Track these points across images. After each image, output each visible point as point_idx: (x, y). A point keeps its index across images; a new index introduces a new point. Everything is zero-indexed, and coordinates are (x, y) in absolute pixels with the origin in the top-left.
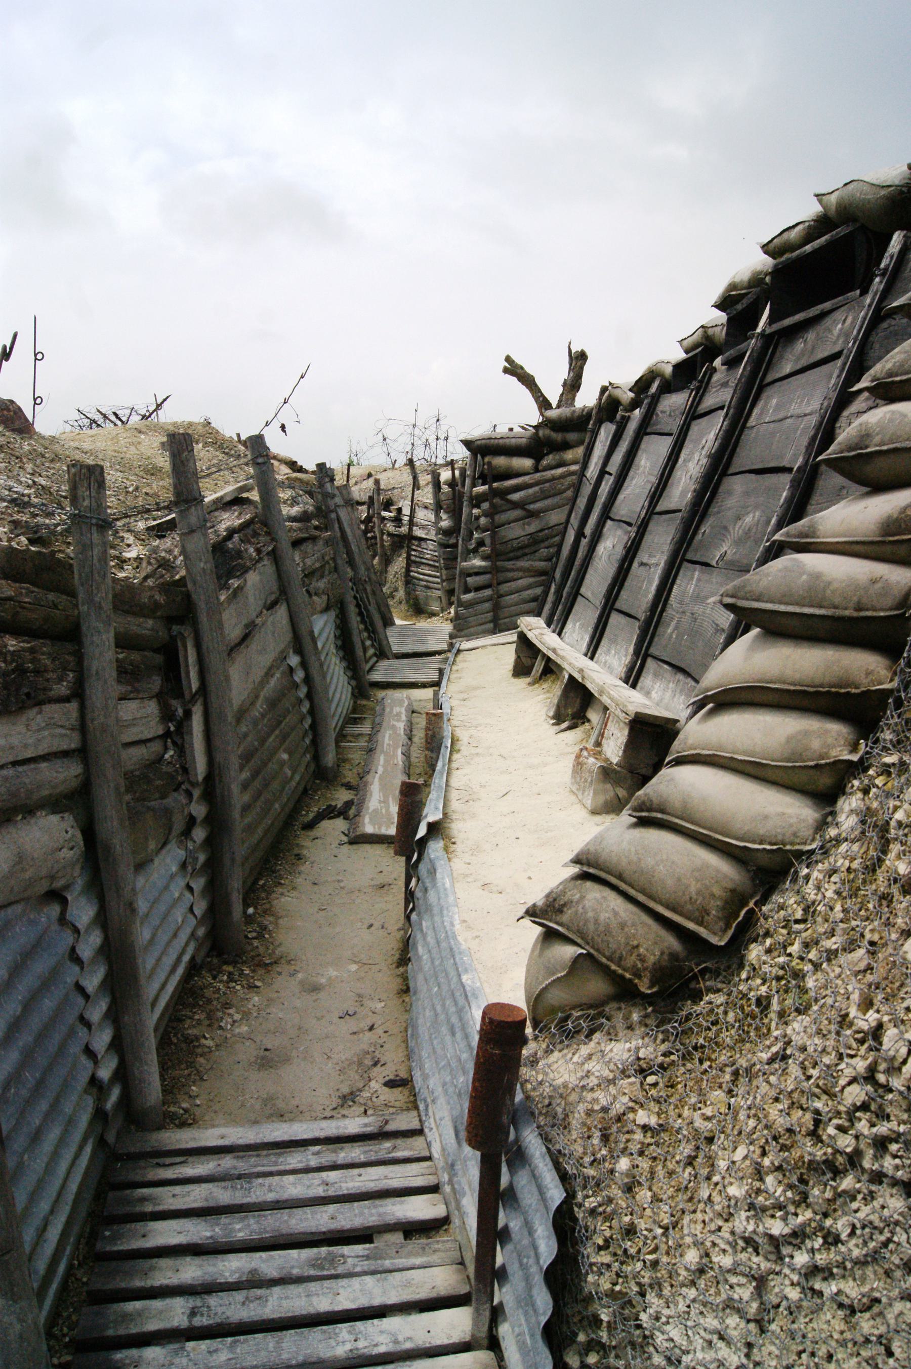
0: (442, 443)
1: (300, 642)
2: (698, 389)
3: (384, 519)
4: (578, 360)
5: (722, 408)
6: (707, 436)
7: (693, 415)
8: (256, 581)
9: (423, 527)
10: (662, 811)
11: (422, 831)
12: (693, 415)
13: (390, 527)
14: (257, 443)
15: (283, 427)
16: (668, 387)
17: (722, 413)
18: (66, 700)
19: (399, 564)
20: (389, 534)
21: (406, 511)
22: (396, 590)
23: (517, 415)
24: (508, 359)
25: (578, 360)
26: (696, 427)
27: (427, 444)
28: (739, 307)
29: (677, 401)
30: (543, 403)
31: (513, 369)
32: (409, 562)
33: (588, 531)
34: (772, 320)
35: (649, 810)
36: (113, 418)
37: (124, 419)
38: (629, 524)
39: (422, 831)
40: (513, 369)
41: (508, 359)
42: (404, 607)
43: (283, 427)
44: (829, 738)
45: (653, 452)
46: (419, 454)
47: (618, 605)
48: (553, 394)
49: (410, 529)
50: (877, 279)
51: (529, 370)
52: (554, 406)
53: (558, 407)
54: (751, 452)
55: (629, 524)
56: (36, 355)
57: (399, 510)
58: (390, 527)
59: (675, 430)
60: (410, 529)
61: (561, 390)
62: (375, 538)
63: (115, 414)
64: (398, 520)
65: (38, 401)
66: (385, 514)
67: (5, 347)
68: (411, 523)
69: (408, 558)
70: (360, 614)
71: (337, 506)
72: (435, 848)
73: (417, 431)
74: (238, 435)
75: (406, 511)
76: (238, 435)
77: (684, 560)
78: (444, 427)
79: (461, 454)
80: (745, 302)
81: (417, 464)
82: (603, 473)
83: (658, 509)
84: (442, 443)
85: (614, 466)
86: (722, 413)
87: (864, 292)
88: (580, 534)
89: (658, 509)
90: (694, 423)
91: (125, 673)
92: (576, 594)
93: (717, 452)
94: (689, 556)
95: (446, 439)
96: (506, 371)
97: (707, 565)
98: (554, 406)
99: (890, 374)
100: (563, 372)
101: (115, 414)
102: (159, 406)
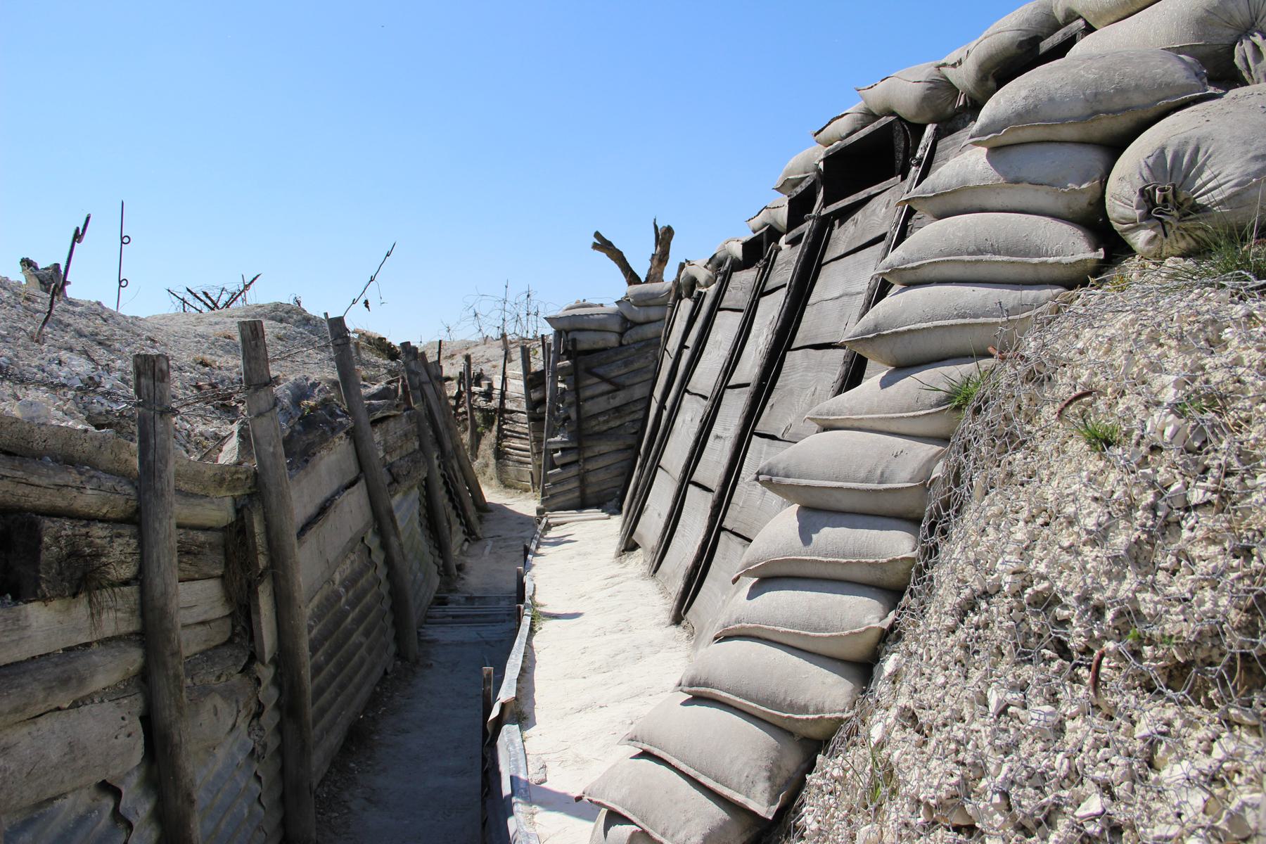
0: (532, 318)
1: (381, 520)
2: (765, 267)
3: (475, 394)
4: (664, 238)
5: (784, 286)
6: (771, 309)
7: (761, 292)
8: (335, 458)
9: (514, 400)
10: (706, 685)
11: (495, 712)
12: (761, 292)
13: (481, 402)
14: (337, 324)
15: (366, 303)
16: (738, 266)
17: (784, 290)
18: (126, 583)
19: (490, 438)
20: (481, 409)
21: (497, 385)
22: (487, 465)
23: (606, 291)
24: (597, 235)
25: (664, 238)
26: (765, 302)
27: (518, 319)
28: (799, 190)
29: (747, 277)
30: (633, 278)
31: (603, 245)
32: (501, 436)
33: (668, 403)
34: (827, 202)
35: (699, 685)
36: (203, 297)
37: (214, 299)
38: (705, 398)
39: (495, 712)
40: (603, 245)
41: (597, 235)
42: (495, 482)
43: (366, 303)
44: (861, 613)
45: (726, 327)
46: (509, 329)
47: (695, 478)
48: (642, 271)
49: (502, 403)
50: (914, 168)
51: (618, 245)
52: (643, 280)
53: (647, 281)
54: (812, 325)
55: (705, 398)
56: (122, 239)
57: (491, 386)
58: (481, 402)
59: (745, 306)
60: (502, 403)
61: (649, 264)
62: (465, 413)
63: (205, 294)
64: (488, 395)
65: (124, 283)
66: (474, 389)
67: (78, 229)
68: (503, 395)
69: (500, 430)
70: (448, 491)
71: (421, 383)
72: (509, 732)
73: (508, 307)
74: (326, 314)
75: (497, 385)
76: (326, 314)
77: (753, 433)
78: (534, 304)
79: (549, 331)
80: (804, 185)
81: (509, 338)
82: (682, 346)
83: (731, 383)
84: (532, 318)
85: (690, 342)
86: (784, 290)
87: (904, 178)
88: (662, 407)
89: (731, 383)
90: (762, 299)
91: (185, 551)
92: (656, 466)
93: (781, 327)
94: (759, 428)
95: (536, 314)
96: (595, 246)
97: (773, 438)
98: (643, 280)
99: (905, 261)
100: (650, 248)
101: (205, 294)
102: (247, 287)
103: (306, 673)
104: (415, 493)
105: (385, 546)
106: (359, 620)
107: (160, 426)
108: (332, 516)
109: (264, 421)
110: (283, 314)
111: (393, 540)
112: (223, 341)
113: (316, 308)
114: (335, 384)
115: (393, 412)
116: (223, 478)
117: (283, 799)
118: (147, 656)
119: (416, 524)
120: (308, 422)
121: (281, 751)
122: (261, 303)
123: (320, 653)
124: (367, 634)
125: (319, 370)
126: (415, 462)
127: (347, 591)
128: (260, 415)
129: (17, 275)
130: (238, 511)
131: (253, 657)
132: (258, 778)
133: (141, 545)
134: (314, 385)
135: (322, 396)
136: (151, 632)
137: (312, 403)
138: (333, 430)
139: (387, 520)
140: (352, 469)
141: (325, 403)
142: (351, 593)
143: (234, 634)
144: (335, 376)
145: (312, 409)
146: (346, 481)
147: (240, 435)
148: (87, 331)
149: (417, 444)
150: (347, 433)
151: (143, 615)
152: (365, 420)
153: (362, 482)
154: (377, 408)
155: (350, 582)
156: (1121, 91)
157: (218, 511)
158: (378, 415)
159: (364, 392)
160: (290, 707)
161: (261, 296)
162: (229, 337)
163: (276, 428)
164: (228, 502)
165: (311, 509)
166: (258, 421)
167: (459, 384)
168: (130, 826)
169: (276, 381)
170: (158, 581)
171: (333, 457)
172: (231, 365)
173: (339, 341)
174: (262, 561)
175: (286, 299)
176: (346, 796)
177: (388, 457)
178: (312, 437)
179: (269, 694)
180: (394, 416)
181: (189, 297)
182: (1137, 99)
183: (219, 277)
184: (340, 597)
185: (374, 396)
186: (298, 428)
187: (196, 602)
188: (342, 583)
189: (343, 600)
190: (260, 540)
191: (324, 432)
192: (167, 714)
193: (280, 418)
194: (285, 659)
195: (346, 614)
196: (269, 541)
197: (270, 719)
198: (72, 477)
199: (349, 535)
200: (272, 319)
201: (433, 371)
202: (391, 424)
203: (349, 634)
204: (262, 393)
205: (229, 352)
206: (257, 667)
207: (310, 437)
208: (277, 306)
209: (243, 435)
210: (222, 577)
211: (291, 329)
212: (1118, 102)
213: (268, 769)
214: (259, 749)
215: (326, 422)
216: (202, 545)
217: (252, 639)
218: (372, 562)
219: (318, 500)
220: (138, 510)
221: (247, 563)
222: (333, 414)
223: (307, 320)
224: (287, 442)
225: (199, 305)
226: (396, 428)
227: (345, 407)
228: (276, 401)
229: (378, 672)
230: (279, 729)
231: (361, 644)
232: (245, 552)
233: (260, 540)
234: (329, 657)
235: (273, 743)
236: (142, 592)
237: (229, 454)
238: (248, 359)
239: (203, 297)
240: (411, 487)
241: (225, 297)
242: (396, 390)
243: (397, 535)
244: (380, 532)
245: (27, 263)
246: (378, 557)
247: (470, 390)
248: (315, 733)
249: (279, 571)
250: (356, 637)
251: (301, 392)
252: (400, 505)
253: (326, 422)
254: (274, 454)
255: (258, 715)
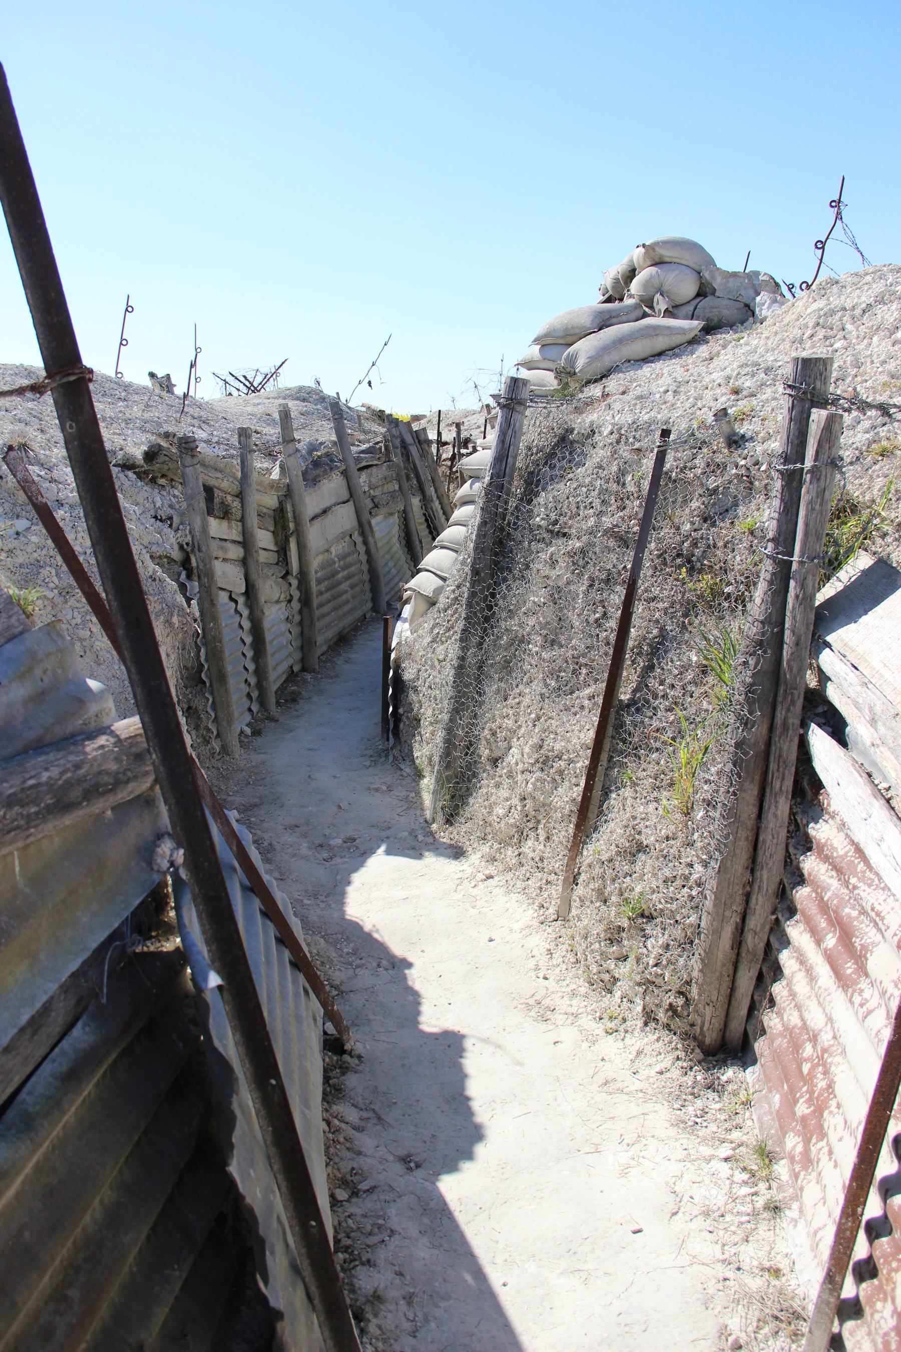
1: (363, 528)
8: (332, 486)
15: (370, 383)
36: (243, 379)
37: (251, 380)
43: (370, 383)
63: (245, 377)
101: (245, 377)
103: (313, 583)
104: (395, 519)
105: (365, 542)
106: (347, 578)
107: (249, 457)
108: (330, 517)
109: (292, 459)
110: (305, 395)
111: (370, 539)
112: (265, 418)
113: (329, 390)
114: (335, 443)
115: (375, 462)
116: (273, 485)
117: (302, 648)
118: (245, 552)
119: (395, 539)
120: (316, 464)
121: (301, 623)
122: (289, 386)
123: (322, 585)
124: (352, 587)
125: (326, 434)
126: (393, 497)
127: (339, 560)
128: (290, 455)
129: (147, 382)
130: (280, 503)
131: (288, 573)
132: (290, 632)
133: (242, 507)
134: (321, 444)
135: (326, 450)
136: (246, 543)
137: (319, 454)
138: (331, 469)
139: (366, 527)
140: (345, 495)
141: (327, 455)
142: (342, 563)
143: (279, 561)
144: (334, 438)
145: (319, 457)
146: (341, 500)
147: (280, 467)
148: (196, 415)
149: (397, 487)
150: (342, 473)
151: (244, 535)
152: (353, 468)
153: (351, 502)
154: (363, 459)
155: (343, 557)
156: (573, 328)
157: (271, 501)
158: (364, 464)
159: (354, 449)
160: (306, 601)
161: (290, 380)
162: (269, 415)
163: (298, 465)
164: (276, 497)
165: (318, 510)
166: (289, 459)
167: (454, 447)
168: (241, 615)
169: (299, 441)
170: (249, 521)
171: (332, 485)
172: (272, 432)
173: (336, 417)
174: (292, 526)
175: (310, 383)
176: (335, 659)
177: (372, 492)
178: (319, 471)
179: (296, 594)
180: (376, 465)
181: (230, 379)
182: (577, 331)
183: (252, 362)
184: (334, 563)
185: (363, 452)
186: (310, 466)
187: (264, 539)
188: (337, 556)
189: (337, 565)
190: (290, 515)
191: (326, 470)
192: (253, 576)
193: (301, 460)
194: (303, 576)
195: (338, 573)
196: (295, 517)
197: (296, 605)
198: (219, 475)
199: (341, 530)
200: (298, 399)
201: (422, 437)
202: (374, 470)
203: (339, 583)
204: (290, 445)
205: (269, 425)
206: (289, 577)
207: (318, 471)
208: (301, 389)
209: (282, 467)
210: (273, 532)
211: (310, 407)
212: (572, 332)
213: (296, 631)
214: (290, 617)
215: (327, 464)
216: (265, 514)
217: (287, 564)
218: (357, 551)
219: (323, 506)
220: (241, 493)
221: (285, 527)
222: (332, 461)
223: (323, 399)
224: (304, 473)
225: (237, 384)
226: (378, 474)
227: (341, 458)
228: (297, 450)
229: (359, 613)
230: (300, 612)
231: (346, 592)
232: (284, 522)
233: (290, 515)
234: (327, 590)
235: (297, 618)
236: (243, 526)
237: (275, 475)
238: (283, 428)
239: (243, 379)
240: (392, 514)
241: (259, 379)
242: (380, 449)
243: (373, 536)
244: (363, 534)
245: (152, 375)
246: (361, 548)
247: (459, 452)
248: (319, 625)
249: (299, 533)
250: (345, 586)
251: (312, 448)
252: (378, 524)
253: (327, 464)
254: (297, 475)
255: (290, 601)
